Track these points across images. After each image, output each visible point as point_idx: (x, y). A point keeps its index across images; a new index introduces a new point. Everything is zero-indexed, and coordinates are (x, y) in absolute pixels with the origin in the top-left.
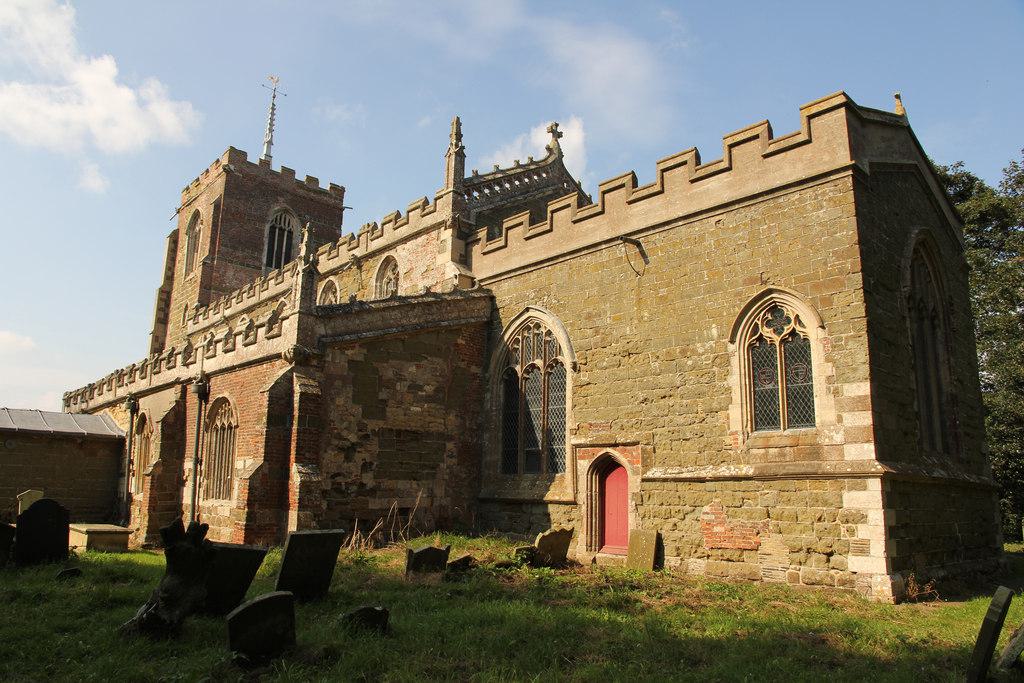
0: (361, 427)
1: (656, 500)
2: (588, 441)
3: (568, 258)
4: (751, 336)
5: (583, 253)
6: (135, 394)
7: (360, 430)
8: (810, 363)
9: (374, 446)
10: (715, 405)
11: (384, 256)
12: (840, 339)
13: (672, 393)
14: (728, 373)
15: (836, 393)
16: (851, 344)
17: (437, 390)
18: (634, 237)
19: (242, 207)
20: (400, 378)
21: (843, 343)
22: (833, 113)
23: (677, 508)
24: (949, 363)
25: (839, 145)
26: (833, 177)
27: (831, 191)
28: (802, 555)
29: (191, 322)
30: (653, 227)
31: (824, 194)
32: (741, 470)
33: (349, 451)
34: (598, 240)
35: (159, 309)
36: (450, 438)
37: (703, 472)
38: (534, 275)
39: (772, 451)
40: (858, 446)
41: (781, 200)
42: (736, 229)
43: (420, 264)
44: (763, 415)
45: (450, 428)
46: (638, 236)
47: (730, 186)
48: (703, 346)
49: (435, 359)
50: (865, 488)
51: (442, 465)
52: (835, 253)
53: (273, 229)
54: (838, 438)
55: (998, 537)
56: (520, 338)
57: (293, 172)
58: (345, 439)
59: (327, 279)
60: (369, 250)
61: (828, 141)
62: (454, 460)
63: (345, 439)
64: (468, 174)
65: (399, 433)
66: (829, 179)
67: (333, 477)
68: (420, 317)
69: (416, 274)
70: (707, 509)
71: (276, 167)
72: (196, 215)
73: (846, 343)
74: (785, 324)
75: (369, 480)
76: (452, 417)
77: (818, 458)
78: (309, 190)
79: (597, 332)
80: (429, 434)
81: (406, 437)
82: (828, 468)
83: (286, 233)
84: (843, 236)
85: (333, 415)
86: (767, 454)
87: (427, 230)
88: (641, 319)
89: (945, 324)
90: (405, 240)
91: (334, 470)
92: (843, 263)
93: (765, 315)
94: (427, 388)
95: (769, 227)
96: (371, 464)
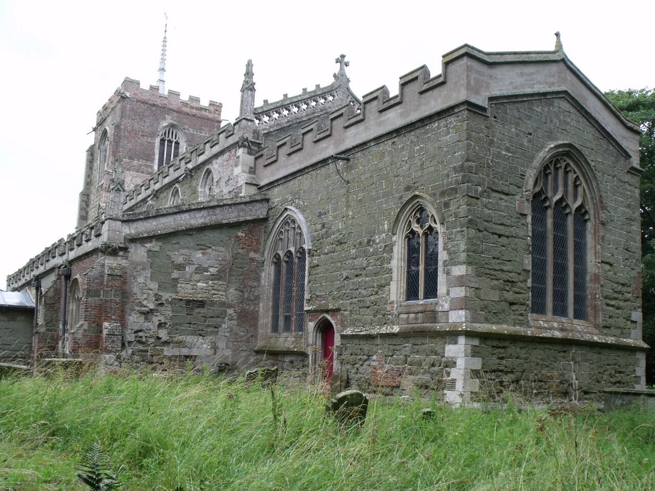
0: (158, 297)
1: (349, 352)
4: (407, 230)
6: (38, 276)
7: (157, 300)
9: (168, 311)
13: (361, 272)
14: (391, 259)
18: (343, 156)
19: (136, 126)
20: (190, 263)
21: (453, 236)
23: (359, 357)
24: (595, 249)
25: (461, 85)
33: (147, 314)
35: (81, 209)
36: (230, 306)
39: (412, 316)
40: (456, 311)
44: (412, 293)
45: (230, 298)
49: (217, 248)
50: (456, 343)
51: (223, 325)
53: (163, 141)
56: (283, 230)
57: (177, 95)
58: (145, 307)
60: (198, 164)
62: (235, 323)
63: (145, 307)
64: (258, 103)
65: (188, 302)
67: (136, 332)
68: (205, 217)
69: (222, 183)
71: (164, 91)
72: (105, 132)
75: (163, 334)
76: (232, 290)
78: (192, 108)
79: (323, 226)
80: (213, 303)
81: (194, 304)
83: (173, 144)
85: (135, 290)
86: (408, 318)
90: (216, 156)
91: (136, 328)
92: (457, 176)
93: (415, 214)
94: (211, 270)
96: (165, 323)
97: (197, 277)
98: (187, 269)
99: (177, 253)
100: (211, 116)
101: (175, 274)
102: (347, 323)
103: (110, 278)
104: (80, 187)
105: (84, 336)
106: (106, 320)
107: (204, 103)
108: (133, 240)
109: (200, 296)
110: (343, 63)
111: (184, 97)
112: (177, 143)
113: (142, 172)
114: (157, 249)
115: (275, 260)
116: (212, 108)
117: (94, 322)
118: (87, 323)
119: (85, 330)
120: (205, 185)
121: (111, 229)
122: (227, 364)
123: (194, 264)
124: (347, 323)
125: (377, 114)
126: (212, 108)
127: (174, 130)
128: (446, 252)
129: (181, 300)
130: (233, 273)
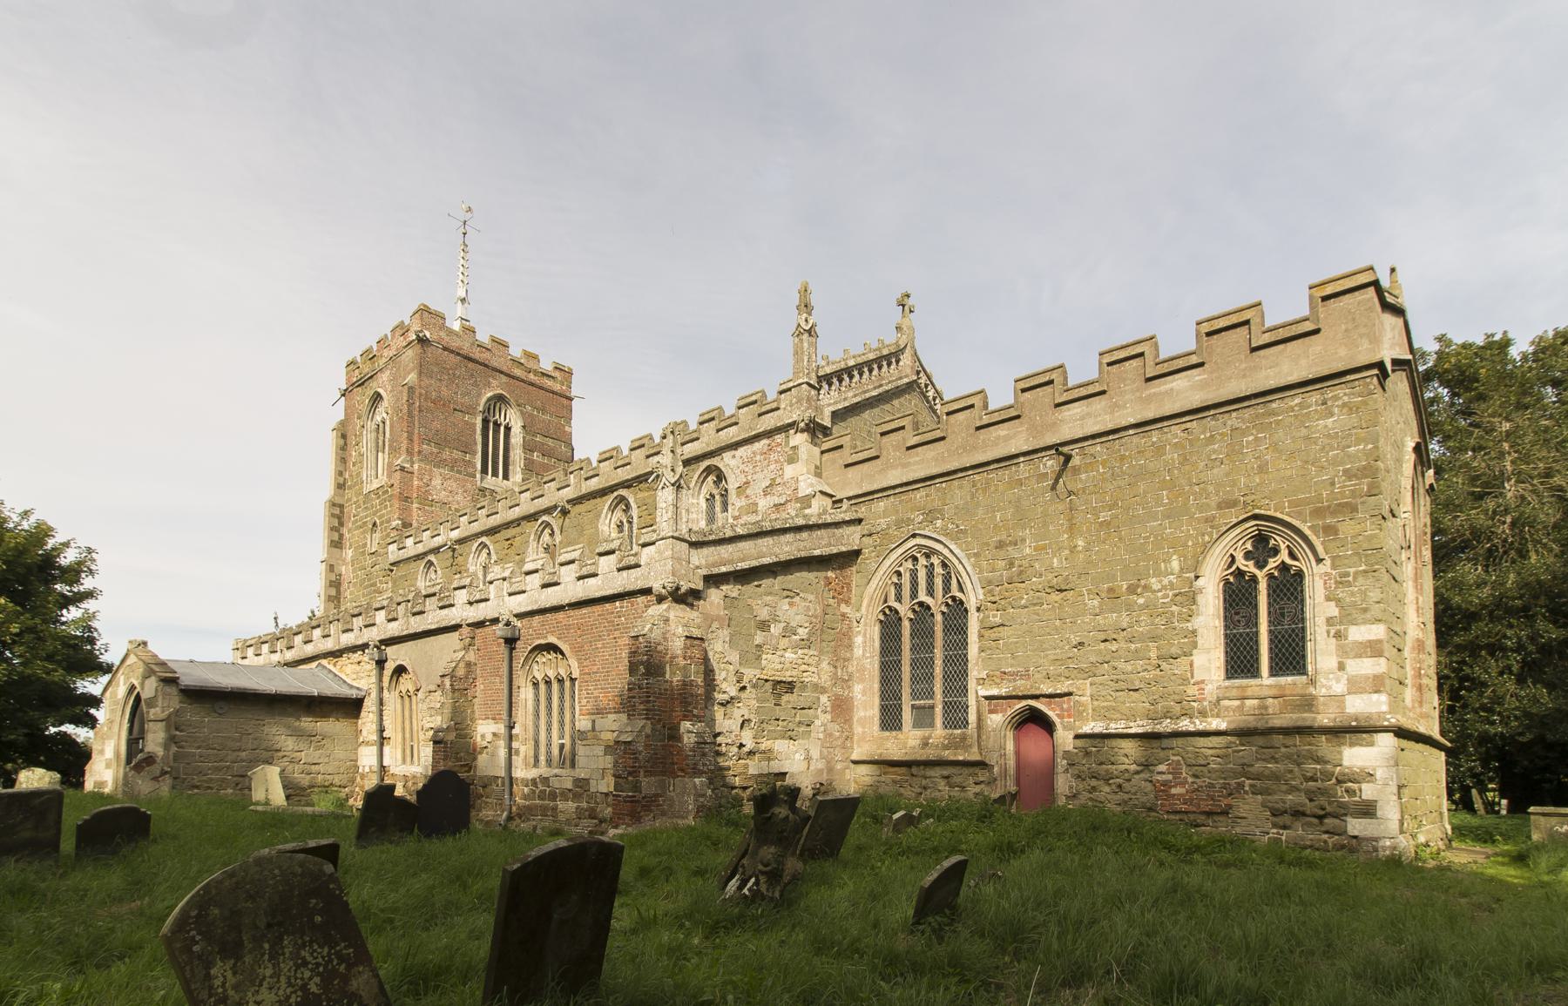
0: (739, 677)
2: (1003, 692)
3: (971, 472)
5: (992, 467)
7: (738, 682)
8: (1303, 601)
10: (1174, 651)
11: (706, 463)
12: (1348, 575)
13: (1115, 636)
15: (1338, 635)
16: (1361, 580)
17: (811, 634)
21: (1351, 579)
22: (1357, 293)
24: (1417, 603)
26: (1349, 378)
27: (1345, 394)
28: (1286, 819)
29: (393, 547)
30: (1093, 437)
31: (1336, 398)
32: (1210, 724)
34: (1014, 451)
36: (823, 690)
37: (1158, 726)
38: (919, 495)
40: (1365, 696)
41: (1274, 405)
42: (1211, 440)
43: (760, 476)
44: (1240, 662)
46: (1071, 447)
47: (1204, 385)
48: (1160, 582)
50: (1371, 744)
52: (1346, 471)
53: (485, 422)
54: (1339, 688)
55: (26, 718)
59: (616, 494)
61: (1346, 330)
62: (829, 717)
66: (1343, 380)
69: (755, 490)
70: (1162, 768)
73: (1355, 578)
74: (1270, 557)
77: (1311, 711)
79: (1011, 564)
80: (804, 686)
82: (1324, 720)
83: (502, 428)
84: (1358, 451)
86: (1243, 706)
87: (768, 434)
88: (1073, 549)
89: (1416, 556)
90: (735, 446)
94: (800, 631)
95: (1257, 439)
97: (784, 643)
98: (772, 630)
99: (760, 602)
100: (557, 387)
101: (759, 638)
102: (1088, 714)
103: (688, 642)
104: (327, 490)
105: (647, 746)
106: (685, 718)
107: (546, 365)
108: (713, 580)
109: (788, 673)
110: (906, 308)
111: (516, 351)
112: (508, 429)
113: (459, 472)
114: (734, 594)
115: (882, 617)
116: (557, 374)
117: (660, 720)
118: (649, 722)
119: (647, 736)
120: (699, 493)
121: (676, 556)
122: (822, 784)
123: (780, 622)
124: (1088, 714)
125: (1140, 382)
126: (557, 374)
127: (503, 406)
128: (1333, 603)
129: (767, 681)
130: (824, 637)
